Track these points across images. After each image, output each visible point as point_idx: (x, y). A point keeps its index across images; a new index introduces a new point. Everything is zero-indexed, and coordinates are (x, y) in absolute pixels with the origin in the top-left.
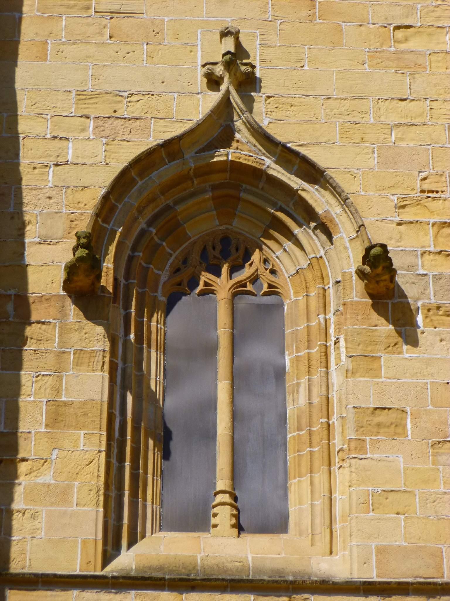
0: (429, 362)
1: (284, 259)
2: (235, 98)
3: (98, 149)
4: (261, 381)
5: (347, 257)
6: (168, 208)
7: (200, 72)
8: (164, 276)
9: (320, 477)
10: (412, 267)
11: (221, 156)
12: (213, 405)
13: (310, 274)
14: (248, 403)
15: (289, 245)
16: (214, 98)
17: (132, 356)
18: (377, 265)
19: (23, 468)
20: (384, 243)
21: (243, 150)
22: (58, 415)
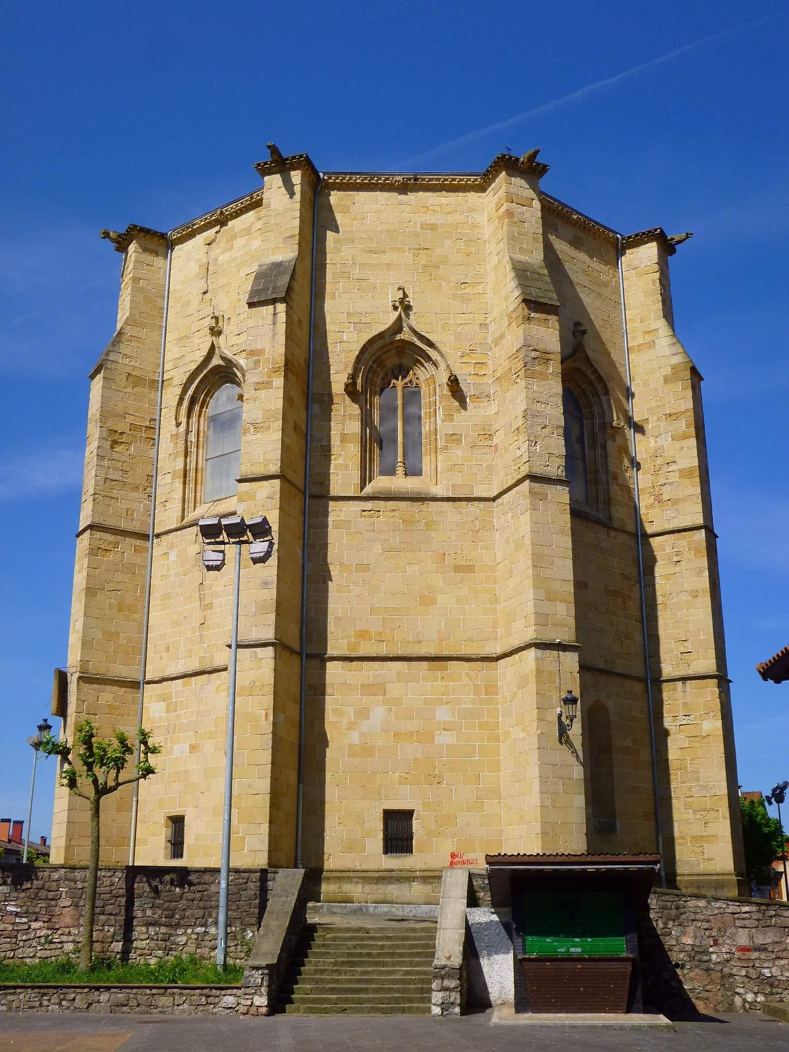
0: (470, 416)
1: (421, 374)
2: (403, 316)
3: (354, 336)
4: (411, 420)
5: (444, 378)
6: (379, 356)
7: (391, 304)
8: (379, 381)
9: (433, 456)
10: (465, 380)
11: (398, 337)
12: (396, 430)
13: (429, 379)
14: (409, 429)
15: (423, 369)
16: (396, 314)
17: (368, 414)
18: (454, 384)
19: (333, 457)
20: (380, 815)
21: (406, 335)
22: (344, 438)
